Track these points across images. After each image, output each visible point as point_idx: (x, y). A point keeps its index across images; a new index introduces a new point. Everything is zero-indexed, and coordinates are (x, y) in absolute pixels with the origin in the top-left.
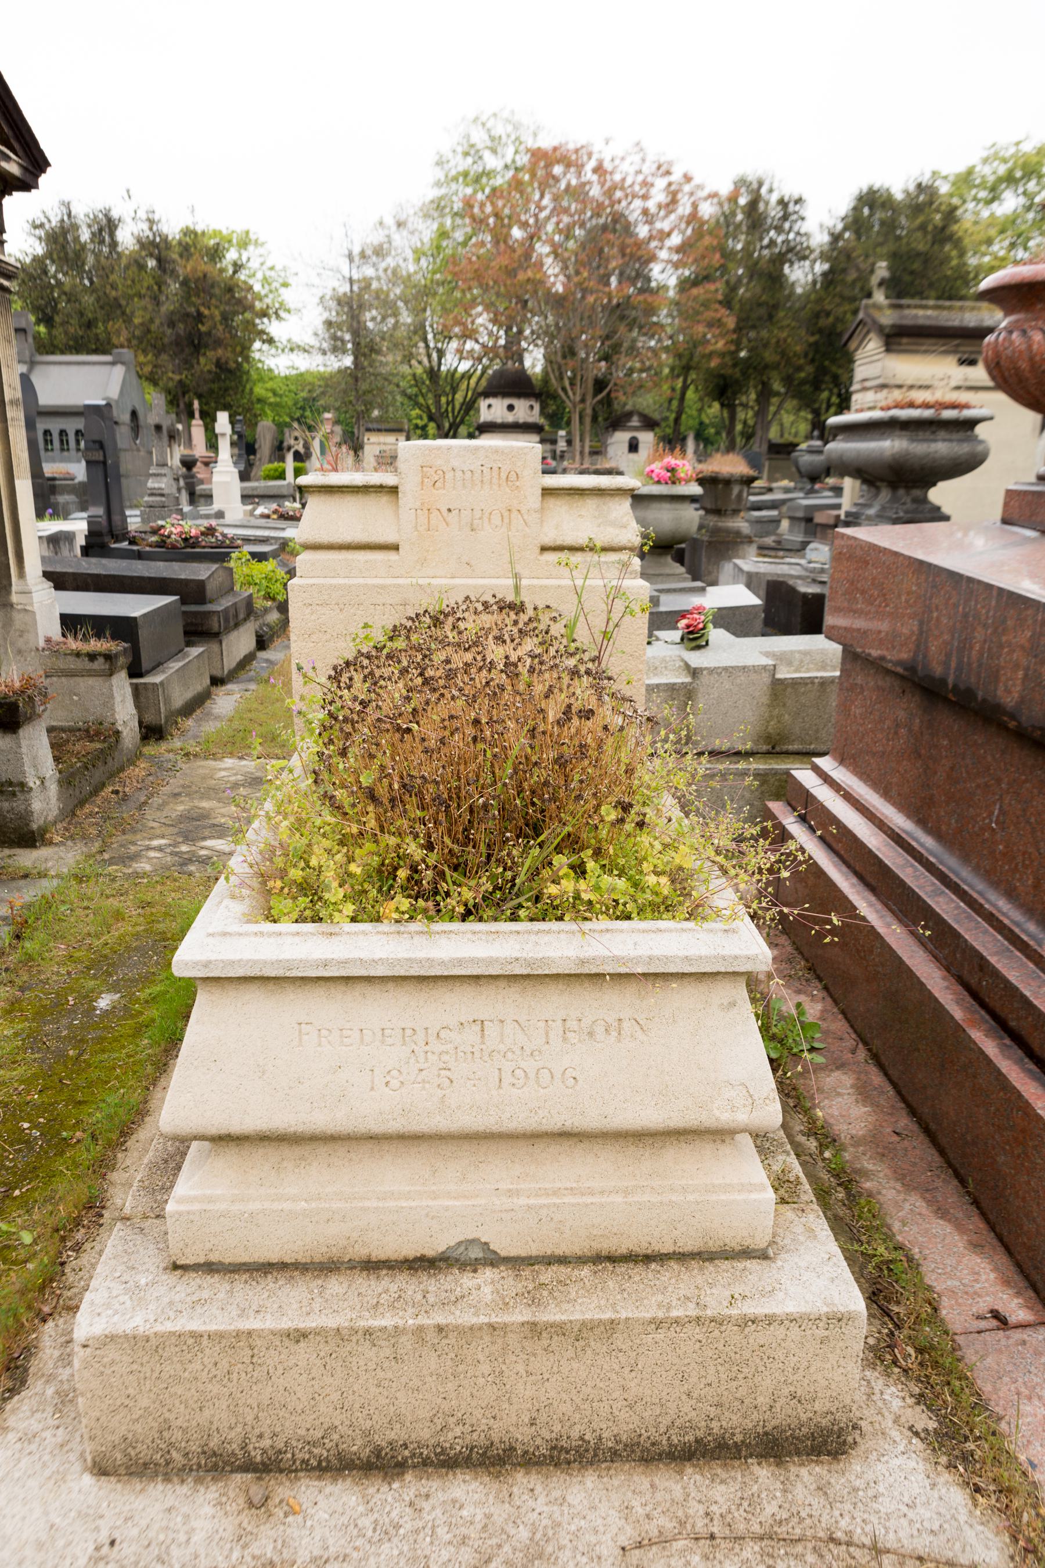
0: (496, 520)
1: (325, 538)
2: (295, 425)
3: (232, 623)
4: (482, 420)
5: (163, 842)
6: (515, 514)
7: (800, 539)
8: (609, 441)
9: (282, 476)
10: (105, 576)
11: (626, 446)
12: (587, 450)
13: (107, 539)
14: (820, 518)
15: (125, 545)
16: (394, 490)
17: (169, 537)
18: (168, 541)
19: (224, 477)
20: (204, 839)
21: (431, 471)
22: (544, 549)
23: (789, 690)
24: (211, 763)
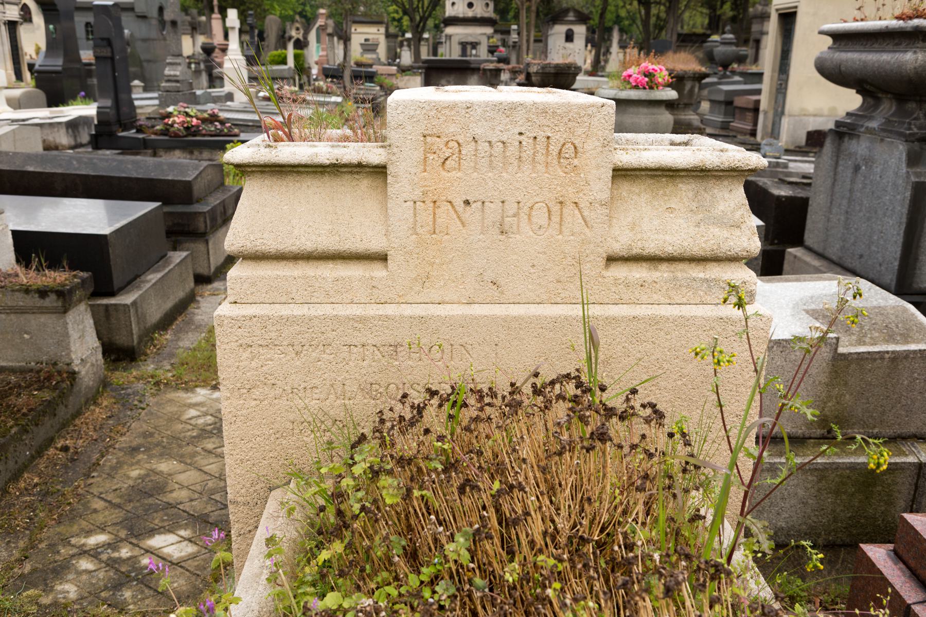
0: (540, 217)
1: (271, 245)
2: (297, 17)
3: (219, 221)
4: (447, 15)
5: (102, 538)
6: (569, 209)
7: (720, 120)
8: (550, 32)
9: (284, 62)
10: (94, 176)
11: (564, 36)
12: (532, 39)
13: (114, 128)
14: (739, 101)
15: (132, 133)
16: (380, 171)
17: (172, 126)
18: (172, 129)
19: (233, 61)
20: (152, 532)
21: (440, 143)
22: (611, 259)
23: (853, 366)
24: (181, 395)
